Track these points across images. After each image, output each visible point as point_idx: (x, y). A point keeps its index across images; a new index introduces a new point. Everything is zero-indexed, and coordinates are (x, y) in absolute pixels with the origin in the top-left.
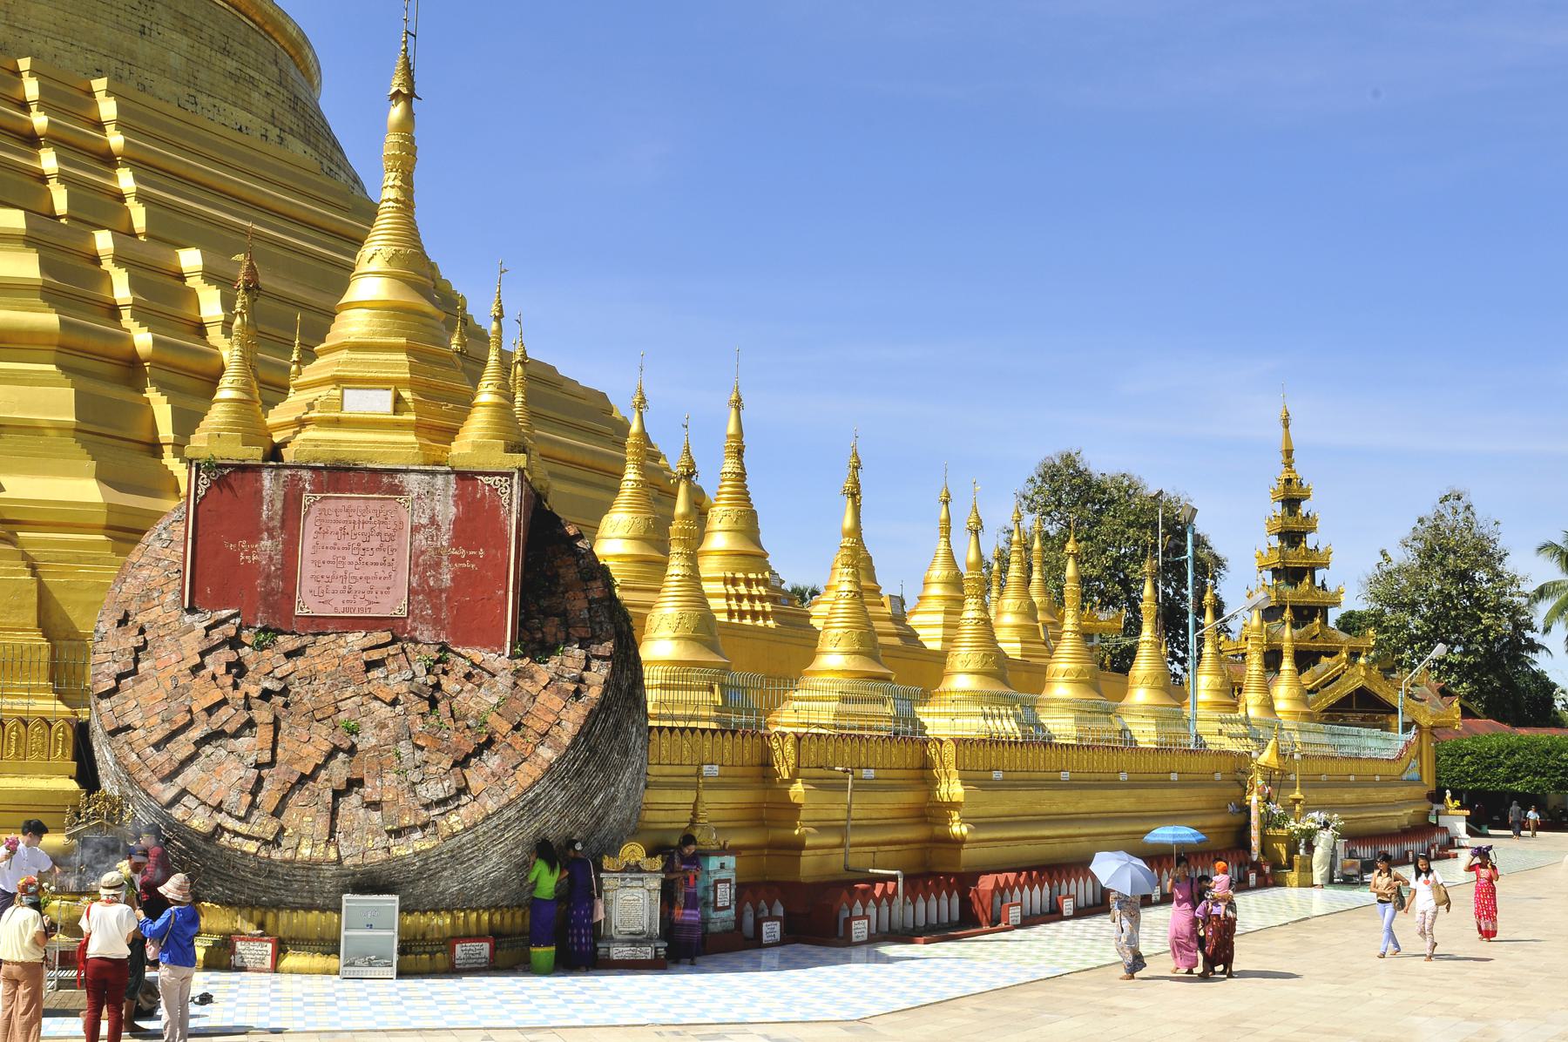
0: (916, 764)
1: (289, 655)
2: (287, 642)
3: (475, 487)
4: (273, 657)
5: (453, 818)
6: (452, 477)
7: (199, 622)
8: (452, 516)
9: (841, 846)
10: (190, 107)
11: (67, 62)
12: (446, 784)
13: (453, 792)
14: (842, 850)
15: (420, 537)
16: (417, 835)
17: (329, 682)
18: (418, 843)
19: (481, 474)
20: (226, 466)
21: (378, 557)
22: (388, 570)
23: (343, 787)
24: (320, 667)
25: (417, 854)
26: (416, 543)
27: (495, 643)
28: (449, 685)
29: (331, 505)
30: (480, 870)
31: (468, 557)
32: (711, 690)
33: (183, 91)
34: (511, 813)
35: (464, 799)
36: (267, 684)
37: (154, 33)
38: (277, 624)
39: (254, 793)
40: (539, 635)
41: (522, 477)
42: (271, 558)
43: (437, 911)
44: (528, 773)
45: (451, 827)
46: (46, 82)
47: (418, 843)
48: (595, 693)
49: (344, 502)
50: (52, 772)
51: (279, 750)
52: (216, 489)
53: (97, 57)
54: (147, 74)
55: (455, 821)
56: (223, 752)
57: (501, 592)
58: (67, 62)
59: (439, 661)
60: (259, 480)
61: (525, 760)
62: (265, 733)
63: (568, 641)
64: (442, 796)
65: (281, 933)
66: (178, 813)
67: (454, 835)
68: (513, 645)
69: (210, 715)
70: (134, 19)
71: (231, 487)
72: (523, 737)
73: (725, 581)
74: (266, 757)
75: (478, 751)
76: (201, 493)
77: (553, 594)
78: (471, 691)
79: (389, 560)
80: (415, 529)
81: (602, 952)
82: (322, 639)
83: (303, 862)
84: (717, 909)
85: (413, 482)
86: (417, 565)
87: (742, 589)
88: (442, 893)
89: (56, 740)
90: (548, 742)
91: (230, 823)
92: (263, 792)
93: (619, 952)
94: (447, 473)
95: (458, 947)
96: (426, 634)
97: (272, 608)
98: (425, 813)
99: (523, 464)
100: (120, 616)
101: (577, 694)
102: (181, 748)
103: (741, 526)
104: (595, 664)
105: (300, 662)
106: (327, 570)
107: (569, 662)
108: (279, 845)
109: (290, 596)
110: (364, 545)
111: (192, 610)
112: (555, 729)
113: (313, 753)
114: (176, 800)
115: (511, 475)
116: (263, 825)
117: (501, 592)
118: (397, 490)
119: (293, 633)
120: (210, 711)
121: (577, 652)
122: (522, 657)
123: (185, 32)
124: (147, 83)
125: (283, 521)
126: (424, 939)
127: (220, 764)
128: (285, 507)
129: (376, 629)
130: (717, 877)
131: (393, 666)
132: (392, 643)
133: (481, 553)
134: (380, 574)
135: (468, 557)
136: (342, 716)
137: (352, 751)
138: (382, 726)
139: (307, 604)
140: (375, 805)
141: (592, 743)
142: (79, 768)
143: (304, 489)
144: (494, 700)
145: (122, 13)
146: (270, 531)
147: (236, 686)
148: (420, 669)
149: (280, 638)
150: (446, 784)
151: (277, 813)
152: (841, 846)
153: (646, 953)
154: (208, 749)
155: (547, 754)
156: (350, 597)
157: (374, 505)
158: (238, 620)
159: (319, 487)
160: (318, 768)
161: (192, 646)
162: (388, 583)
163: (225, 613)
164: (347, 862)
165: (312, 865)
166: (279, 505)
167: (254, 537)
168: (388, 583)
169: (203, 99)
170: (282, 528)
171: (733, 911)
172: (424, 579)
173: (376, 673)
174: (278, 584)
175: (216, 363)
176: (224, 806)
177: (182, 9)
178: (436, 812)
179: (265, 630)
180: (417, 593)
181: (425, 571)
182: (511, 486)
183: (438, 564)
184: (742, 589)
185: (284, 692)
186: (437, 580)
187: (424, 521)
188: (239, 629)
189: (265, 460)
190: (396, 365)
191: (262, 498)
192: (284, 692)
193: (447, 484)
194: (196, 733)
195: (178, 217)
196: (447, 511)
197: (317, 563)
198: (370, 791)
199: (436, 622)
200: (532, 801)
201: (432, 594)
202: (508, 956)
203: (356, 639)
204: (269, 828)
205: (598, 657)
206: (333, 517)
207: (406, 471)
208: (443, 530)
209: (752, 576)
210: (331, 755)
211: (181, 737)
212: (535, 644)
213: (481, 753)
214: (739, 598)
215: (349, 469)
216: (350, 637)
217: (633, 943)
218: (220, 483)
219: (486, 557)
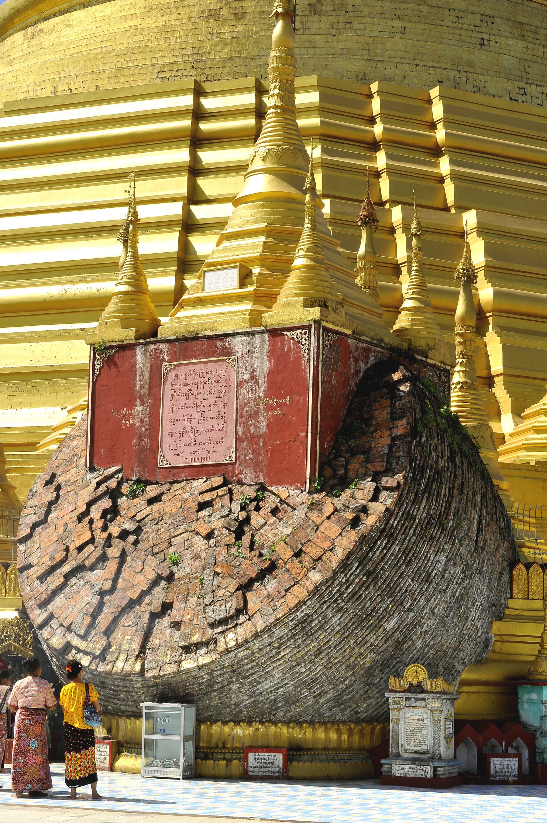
1: (151, 502)
2: (152, 491)
3: (283, 342)
4: (140, 502)
5: (231, 635)
6: (266, 335)
7: (93, 478)
8: (266, 370)
10: (520, 98)
11: (415, 80)
12: (228, 605)
13: (233, 612)
15: (244, 391)
16: (203, 651)
17: (169, 522)
18: (204, 658)
20: (111, 348)
22: (222, 422)
23: (158, 610)
24: (167, 510)
25: (200, 668)
26: (241, 397)
27: (296, 480)
28: (256, 519)
29: (182, 370)
30: (266, 685)
31: (278, 405)
33: (512, 86)
34: (281, 631)
35: (242, 618)
37: (492, 43)
38: (146, 476)
39: (94, 616)
40: (341, 472)
41: (318, 329)
42: (142, 420)
43: (237, 722)
44: (300, 592)
45: (226, 643)
46: (450, 102)
47: (204, 658)
48: (370, 521)
49: (191, 368)
51: (120, 580)
52: (106, 367)
53: (438, 71)
54: (481, 77)
55: (231, 639)
56: (82, 582)
57: (303, 434)
58: (415, 80)
59: (256, 499)
60: (134, 356)
61: (296, 583)
62: (112, 565)
63: (364, 477)
64: (223, 616)
65: (120, 738)
67: (228, 651)
68: (312, 481)
69: (79, 553)
70: (474, 35)
71: (116, 365)
72: (300, 562)
74: (108, 585)
75: (261, 576)
76: (97, 372)
77: (364, 434)
78: (274, 523)
79: (222, 414)
80: (240, 385)
81: (385, 768)
82: (176, 486)
83: (117, 674)
85: (238, 344)
86: (242, 416)
88: (237, 705)
89: (10, 580)
90: (319, 566)
91: (76, 642)
92: (102, 615)
93: (401, 769)
94: (263, 332)
95: (251, 756)
96: (249, 476)
97: (142, 462)
98: (210, 632)
99: (317, 316)
100: (48, 478)
101: (355, 523)
102: (56, 580)
104: (383, 494)
105: (156, 507)
107: (359, 494)
108: (105, 659)
109: (154, 451)
110: (205, 403)
111: (92, 469)
112: (328, 554)
115: (308, 327)
116: (96, 644)
117: (303, 434)
118: (227, 352)
119: (157, 483)
120: (80, 549)
121: (369, 485)
122: (319, 491)
123: (523, 38)
124: (482, 85)
125: (150, 388)
126: (224, 747)
127: (77, 592)
128: (151, 377)
131: (217, 505)
133: (288, 400)
134: (216, 426)
135: (278, 405)
136: (172, 550)
138: (196, 557)
139: (168, 457)
140: (176, 625)
141: (369, 567)
143: (163, 359)
144: (288, 531)
145: (464, 32)
146: (141, 397)
147: (105, 528)
148: (236, 507)
149: (149, 488)
150: (228, 605)
151: (108, 633)
153: (426, 771)
154: (73, 581)
155: (316, 577)
156: (195, 449)
157: (211, 367)
158: (121, 475)
159: (174, 357)
160: (144, 594)
161: (86, 495)
162: (221, 434)
164: (149, 674)
165: (125, 677)
166: (147, 375)
167: (131, 405)
168: (221, 434)
169: (532, 89)
170: (149, 394)
172: (247, 428)
173: (205, 513)
174: (146, 442)
175: (398, 296)
176: (72, 627)
177: (520, 18)
178: (218, 630)
179: (138, 482)
180: (242, 441)
181: (247, 422)
182: (309, 337)
183: (257, 414)
185: (138, 531)
186: (257, 428)
187: (246, 377)
188: (120, 484)
189: (137, 339)
190: (254, 246)
191: (136, 370)
192: (138, 531)
193: (263, 341)
194: (66, 568)
195: (529, 196)
196: (263, 365)
197: (173, 422)
198: (175, 614)
199: (256, 465)
200: (302, 622)
201: (252, 439)
202: (299, 765)
203: (198, 485)
205: (387, 489)
206: (183, 381)
207: (233, 335)
208: (260, 383)
211: (58, 572)
212: (331, 478)
213: (263, 578)
215: (193, 339)
216: (195, 483)
217: (414, 761)
218: (110, 362)
219: (292, 402)
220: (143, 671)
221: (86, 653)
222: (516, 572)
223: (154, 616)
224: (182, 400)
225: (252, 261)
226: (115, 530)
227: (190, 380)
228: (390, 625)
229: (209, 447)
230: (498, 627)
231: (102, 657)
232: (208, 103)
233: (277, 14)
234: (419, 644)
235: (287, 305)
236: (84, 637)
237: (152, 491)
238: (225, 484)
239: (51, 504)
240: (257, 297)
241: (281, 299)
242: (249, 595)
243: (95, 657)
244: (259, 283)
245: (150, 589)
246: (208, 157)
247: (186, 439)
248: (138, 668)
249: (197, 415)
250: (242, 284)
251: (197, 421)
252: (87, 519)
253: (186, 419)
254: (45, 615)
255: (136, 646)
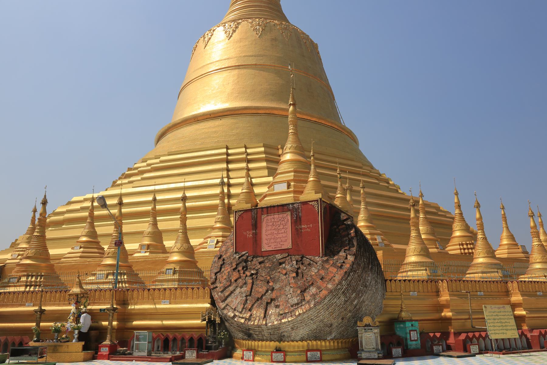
0: (503, 290)
1: (260, 263)
9: (469, 319)
14: (470, 321)
19: (310, 201)
20: (240, 211)
21: (283, 231)
22: (286, 234)
31: (307, 227)
32: (426, 270)
36: (252, 272)
48: (347, 266)
50: (204, 302)
66: (225, 312)
73: (460, 245)
81: (359, 355)
84: (411, 341)
87: (465, 246)
99: (321, 197)
103: (464, 228)
106: (269, 237)
111: (236, 253)
113: (262, 290)
114: (224, 309)
115: (317, 201)
129: (283, 253)
130: (411, 329)
131: (266, 261)
132: (288, 256)
135: (307, 227)
137: (273, 289)
139: (265, 247)
142: (211, 301)
147: (244, 273)
152: (469, 319)
157: (281, 216)
162: (286, 238)
163: (245, 252)
165: (259, 326)
168: (286, 238)
171: (419, 341)
184: (465, 246)
185: (257, 274)
190: (291, 176)
192: (257, 274)
203: (279, 256)
204: (247, 315)
209: (468, 242)
210: (267, 291)
214: (464, 249)
220: (266, 324)
221: (243, 318)
222: (387, 283)
223: (268, 303)
224: (270, 228)
225: (291, 180)
226: (248, 273)
227: (273, 220)
228: (355, 303)
229: (282, 243)
230: (385, 302)
231: (249, 319)
232: (230, 151)
233: (290, 104)
234: (364, 309)
235: (308, 193)
236: (241, 312)
237: (260, 259)
238: (288, 256)
239: (221, 265)
240: (295, 192)
241: (306, 191)
242: (305, 294)
243: (246, 319)
244: (294, 187)
245: (265, 294)
246: (231, 166)
247: (272, 241)
248: (264, 323)
249: (276, 232)
250: (288, 188)
251: (276, 235)
252: (237, 270)
253: (272, 234)
254: (225, 305)
255: (262, 315)
